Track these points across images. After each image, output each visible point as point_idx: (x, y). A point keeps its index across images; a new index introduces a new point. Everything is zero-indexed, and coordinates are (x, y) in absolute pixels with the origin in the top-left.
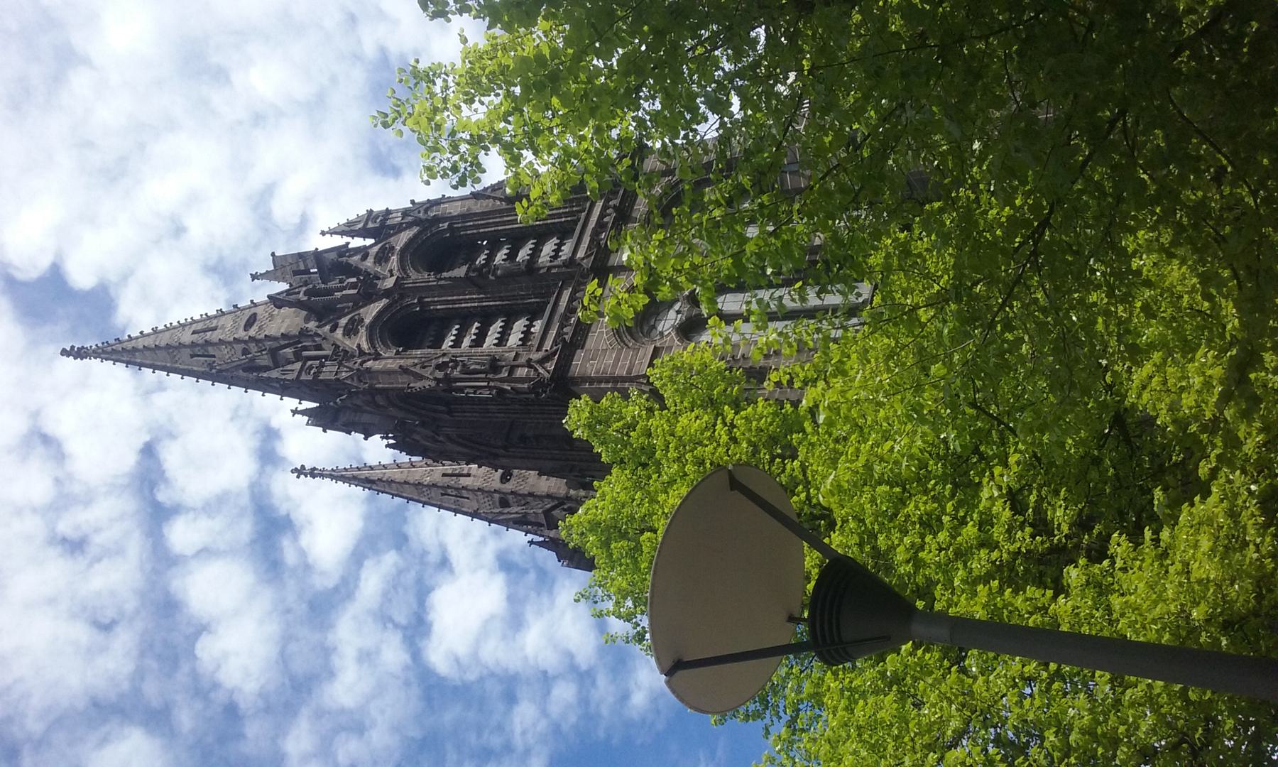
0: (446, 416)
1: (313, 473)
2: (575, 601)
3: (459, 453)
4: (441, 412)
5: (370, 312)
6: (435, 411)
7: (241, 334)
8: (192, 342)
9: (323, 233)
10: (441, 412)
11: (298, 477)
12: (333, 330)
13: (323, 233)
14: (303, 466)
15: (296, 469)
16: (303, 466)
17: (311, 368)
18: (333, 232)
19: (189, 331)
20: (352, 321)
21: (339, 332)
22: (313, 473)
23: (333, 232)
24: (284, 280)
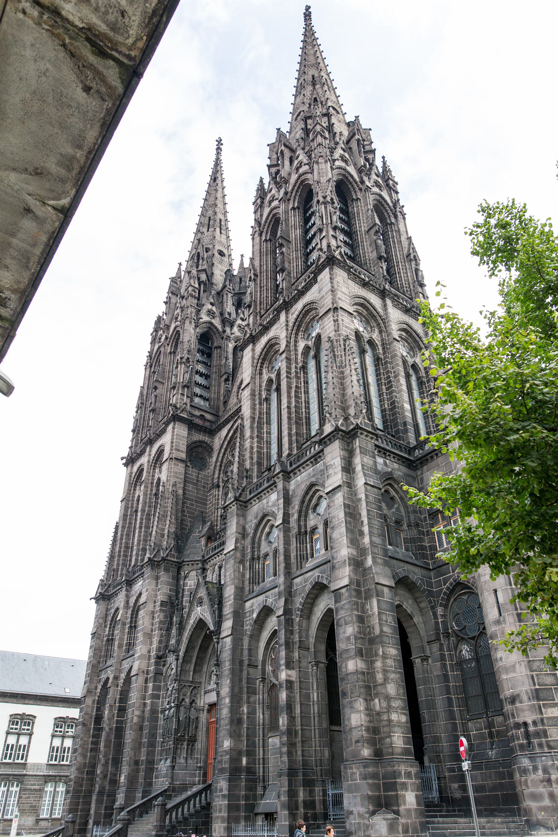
0: (291, 206)
1: (219, 149)
2: (309, 7)
3: (261, 215)
4: (294, 204)
5: (217, 322)
6: (294, 201)
7: (217, 247)
8: (166, 303)
9: (383, 157)
10: (294, 204)
11: (217, 141)
12: (212, 304)
13: (383, 157)
14: (222, 144)
15: (221, 140)
16: (222, 144)
17: (195, 292)
18: (384, 163)
19: (222, 217)
20: (214, 313)
21: (210, 307)
22: (219, 149)
23: (384, 163)
24: (239, 272)
